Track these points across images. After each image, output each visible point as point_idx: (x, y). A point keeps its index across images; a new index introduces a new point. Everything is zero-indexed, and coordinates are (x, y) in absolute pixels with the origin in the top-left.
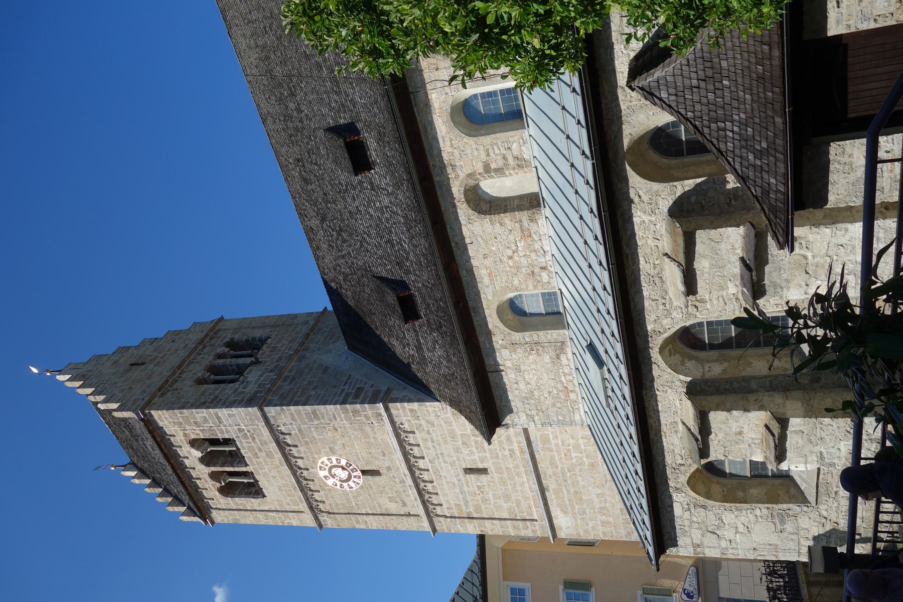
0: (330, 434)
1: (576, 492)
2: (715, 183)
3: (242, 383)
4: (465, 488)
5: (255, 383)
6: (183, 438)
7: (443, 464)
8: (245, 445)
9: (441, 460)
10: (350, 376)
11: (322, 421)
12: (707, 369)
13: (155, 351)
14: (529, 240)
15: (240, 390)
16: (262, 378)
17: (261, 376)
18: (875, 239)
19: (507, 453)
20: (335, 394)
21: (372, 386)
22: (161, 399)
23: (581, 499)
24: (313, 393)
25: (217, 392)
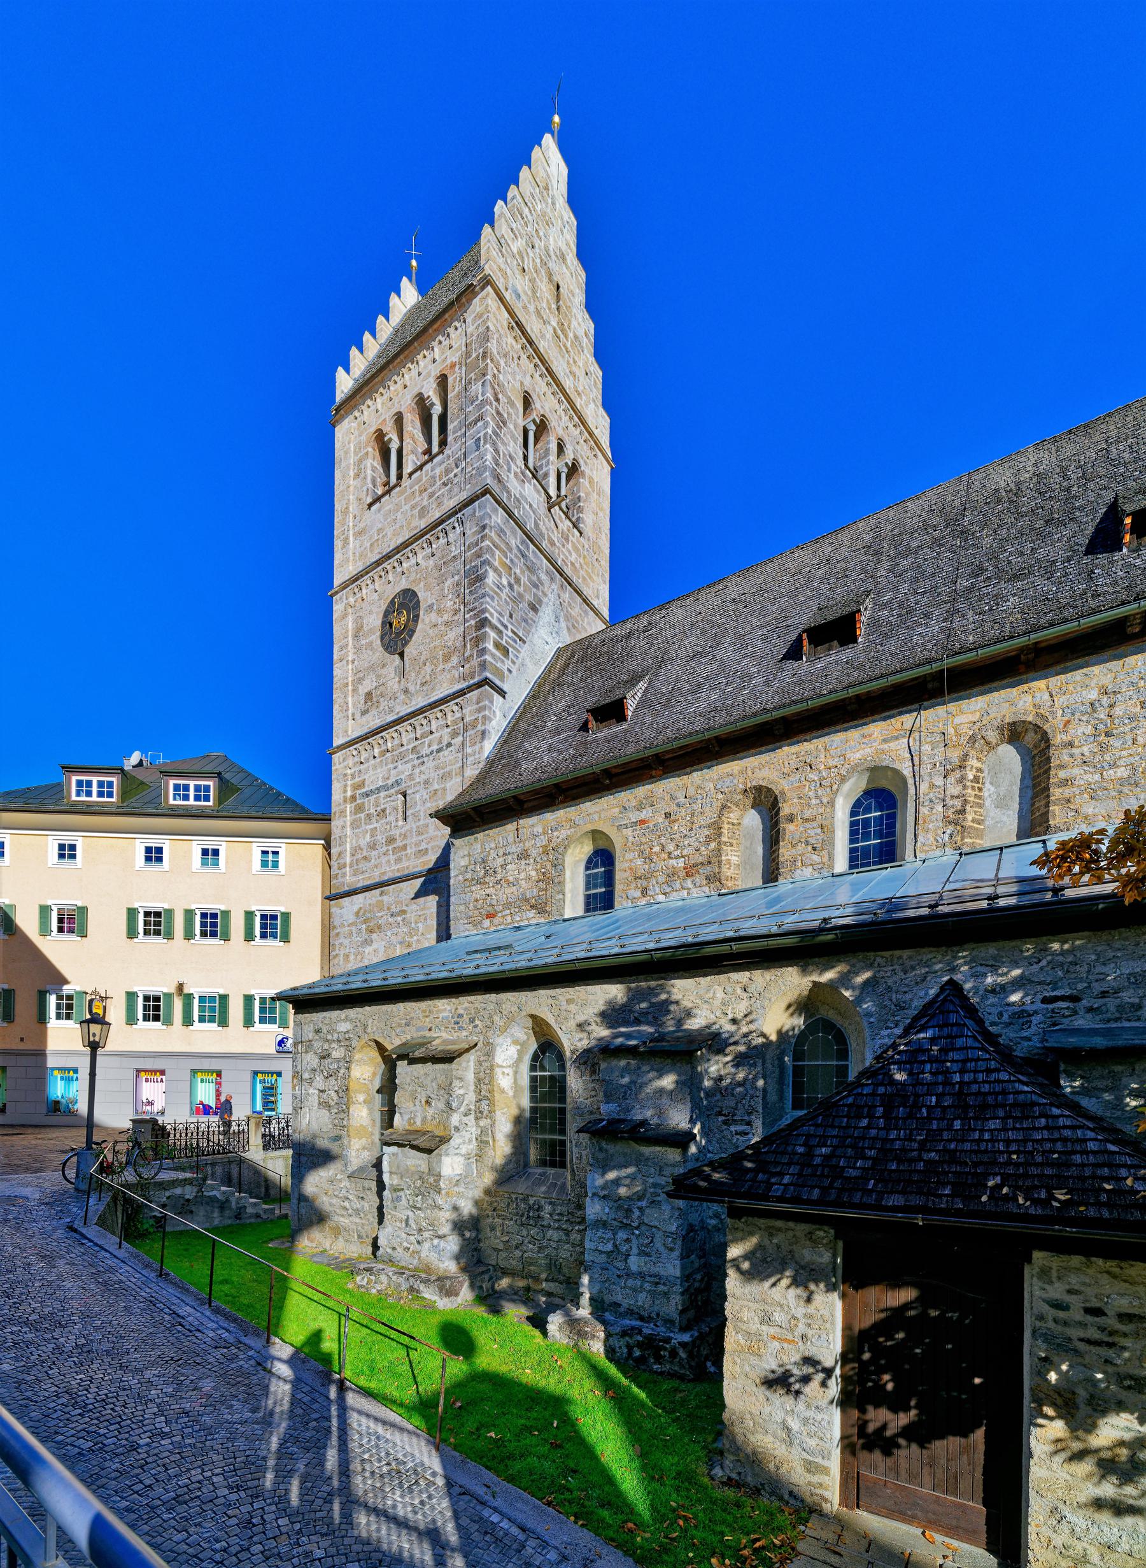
0: (449, 604)
1: (379, 927)
2: (752, 1097)
3: (523, 473)
4: (383, 794)
5: (521, 494)
6: (448, 362)
7: (409, 765)
8: (437, 471)
9: (416, 762)
10: (524, 642)
11: (467, 591)
12: (507, 1071)
13: (576, 337)
14: (682, 874)
15: (513, 467)
16: (527, 507)
17: (531, 506)
18: (336, 707)
19: (423, 846)
20: (500, 614)
21: (510, 671)
22: (505, 324)
23: (372, 932)
24: (505, 582)
25: (512, 427)
